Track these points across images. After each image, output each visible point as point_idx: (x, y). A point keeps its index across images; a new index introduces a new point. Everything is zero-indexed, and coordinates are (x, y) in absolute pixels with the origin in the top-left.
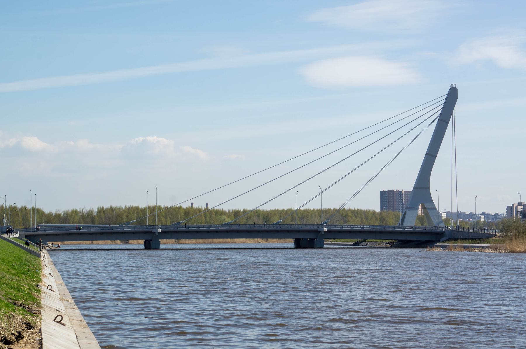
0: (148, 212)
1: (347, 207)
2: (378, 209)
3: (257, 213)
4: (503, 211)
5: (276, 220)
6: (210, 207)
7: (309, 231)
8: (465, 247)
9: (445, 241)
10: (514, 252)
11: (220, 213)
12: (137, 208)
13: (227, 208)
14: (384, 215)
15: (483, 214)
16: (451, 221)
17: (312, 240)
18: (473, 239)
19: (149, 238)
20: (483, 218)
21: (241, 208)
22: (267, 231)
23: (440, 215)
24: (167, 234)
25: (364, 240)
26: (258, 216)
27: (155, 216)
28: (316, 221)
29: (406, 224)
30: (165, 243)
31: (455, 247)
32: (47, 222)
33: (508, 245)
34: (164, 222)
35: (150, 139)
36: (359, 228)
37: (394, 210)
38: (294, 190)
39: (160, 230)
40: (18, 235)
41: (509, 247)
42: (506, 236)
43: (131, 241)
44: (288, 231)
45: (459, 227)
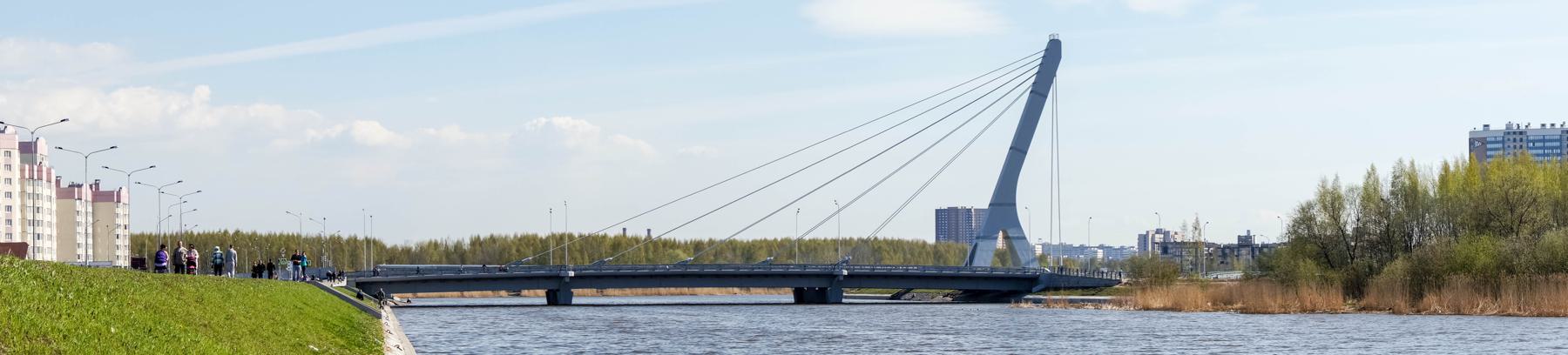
0: (552, 243)
1: (880, 236)
2: (931, 239)
3: (732, 245)
4: (1132, 243)
5: (762, 257)
6: (654, 235)
7: (817, 276)
8: (1071, 301)
9: (1039, 292)
10: (1147, 309)
11: (672, 245)
12: (535, 237)
13: (683, 236)
14: (941, 249)
15: (1101, 247)
16: (1050, 259)
17: (823, 290)
18: (1084, 288)
19: (553, 285)
20: (1100, 254)
21: (705, 237)
22: (749, 276)
23: (1033, 250)
24: (583, 280)
25: (908, 291)
26: (734, 250)
27: (563, 249)
28: (829, 258)
29: (976, 263)
30: (581, 296)
31: (1056, 301)
32: (390, 261)
33: (1139, 298)
34: (579, 261)
35: (561, 121)
36: (900, 270)
37: (957, 240)
38: (794, 208)
39: (572, 274)
40: (344, 283)
41: (1140, 302)
42: (1137, 283)
43: (525, 292)
44: (783, 276)
45: (1061, 269)
